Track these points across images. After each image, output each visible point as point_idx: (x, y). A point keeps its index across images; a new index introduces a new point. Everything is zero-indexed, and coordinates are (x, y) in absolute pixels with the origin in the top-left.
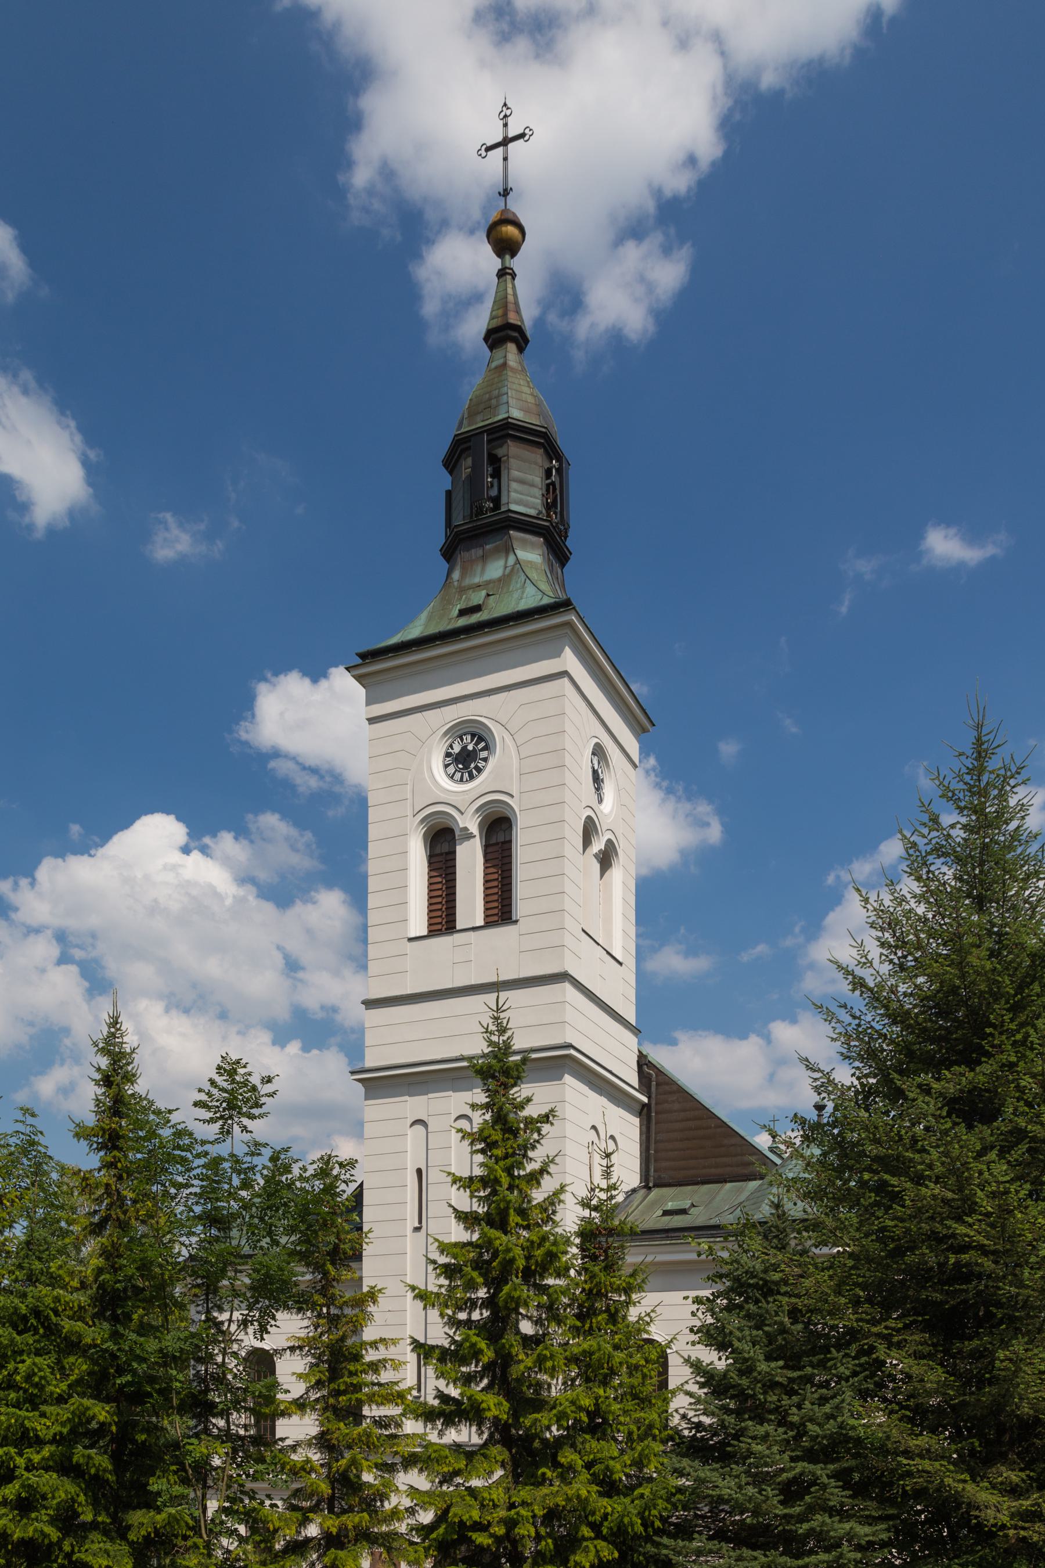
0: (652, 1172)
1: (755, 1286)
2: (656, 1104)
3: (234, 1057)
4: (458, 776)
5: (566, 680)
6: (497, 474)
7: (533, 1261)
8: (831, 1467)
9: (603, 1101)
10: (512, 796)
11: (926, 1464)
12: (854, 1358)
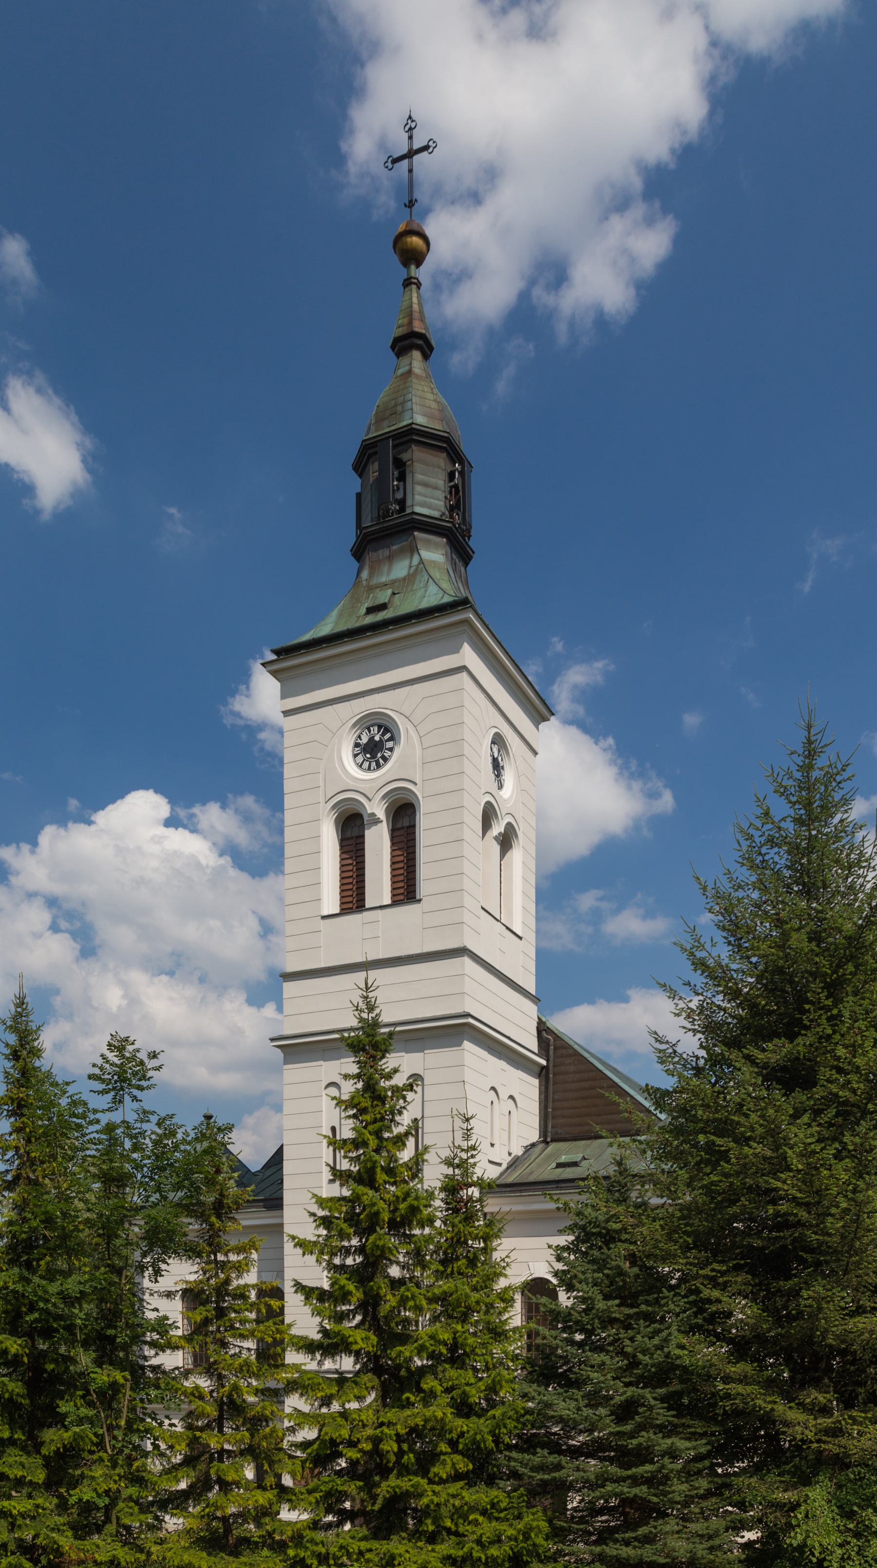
0: (550, 1129)
1: (599, 1234)
2: (554, 1066)
3: (123, 1035)
4: (366, 765)
5: (465, 674)
6: (402, 478)
7: (397, 1214)
8: (659, 1391)
9: (503, 1064)
10: (415, 784)
11: (740, 1388)
12: (684, 1297)
